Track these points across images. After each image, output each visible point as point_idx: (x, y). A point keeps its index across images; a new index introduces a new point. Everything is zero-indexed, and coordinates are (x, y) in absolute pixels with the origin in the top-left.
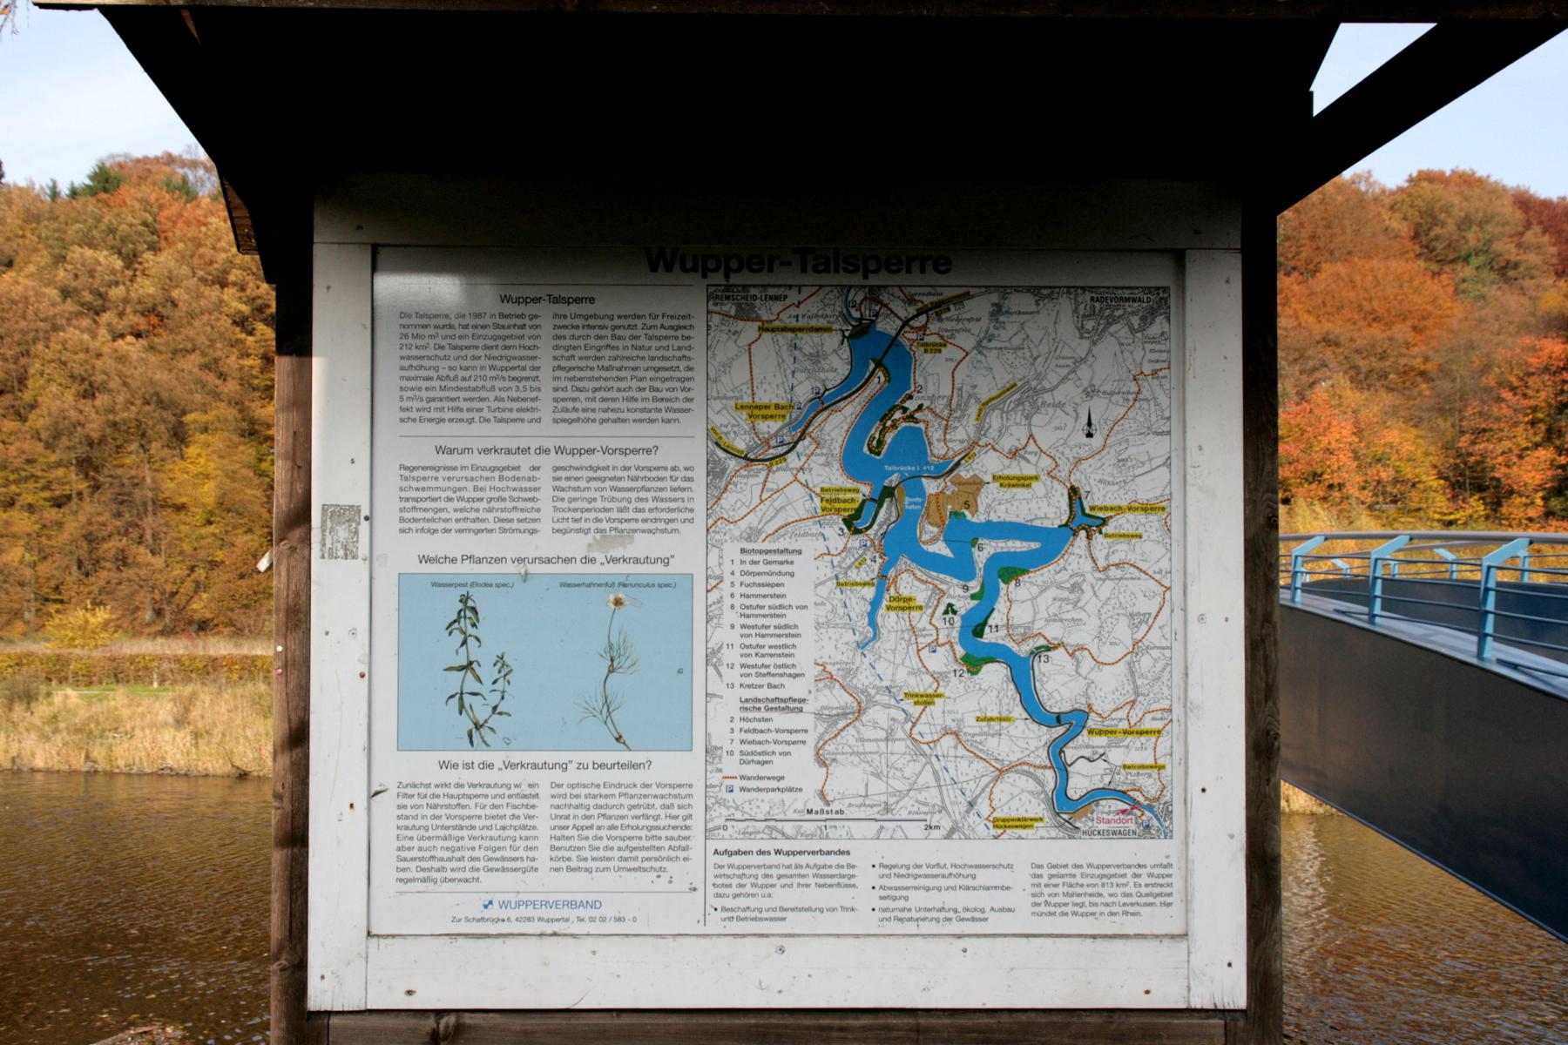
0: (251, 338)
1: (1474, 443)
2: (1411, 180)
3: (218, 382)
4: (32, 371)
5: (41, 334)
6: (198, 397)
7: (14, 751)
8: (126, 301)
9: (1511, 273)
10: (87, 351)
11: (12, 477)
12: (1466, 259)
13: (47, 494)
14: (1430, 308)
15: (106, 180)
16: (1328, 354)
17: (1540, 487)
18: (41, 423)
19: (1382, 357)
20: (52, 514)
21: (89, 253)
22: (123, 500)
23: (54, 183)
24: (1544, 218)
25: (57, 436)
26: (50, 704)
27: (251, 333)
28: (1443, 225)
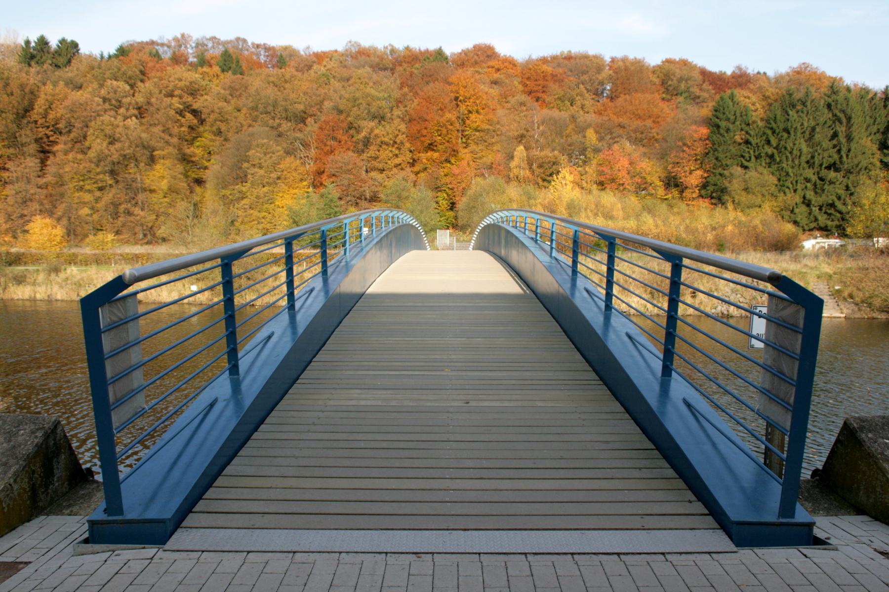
0: (183, 119)
1: (673, 168)
2: (663, 62)
3: (169, 138)
4: (89, 133)
5: (92, 118)
6: (161, 145)
7: (49, 293)
8: (130, 104)
9: (697, 101)
10: (113, 125)
11: (81, 178)
12: (681, 94)
13: (96, 185)
14: (660, 114)
15: (123, 52)
16: (621, 131)
17: (697, 186)
18: (93, 155)
19: (642, 133)
20: (98, 194)
21: (115, 83)
22: (129, 187)
23: (102, 52)
24: (710, 79)
25: (99, 161)
26: (66, 273)
27: (184, 117)
28: (672, 80)
